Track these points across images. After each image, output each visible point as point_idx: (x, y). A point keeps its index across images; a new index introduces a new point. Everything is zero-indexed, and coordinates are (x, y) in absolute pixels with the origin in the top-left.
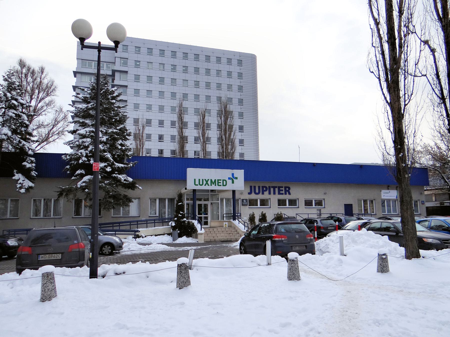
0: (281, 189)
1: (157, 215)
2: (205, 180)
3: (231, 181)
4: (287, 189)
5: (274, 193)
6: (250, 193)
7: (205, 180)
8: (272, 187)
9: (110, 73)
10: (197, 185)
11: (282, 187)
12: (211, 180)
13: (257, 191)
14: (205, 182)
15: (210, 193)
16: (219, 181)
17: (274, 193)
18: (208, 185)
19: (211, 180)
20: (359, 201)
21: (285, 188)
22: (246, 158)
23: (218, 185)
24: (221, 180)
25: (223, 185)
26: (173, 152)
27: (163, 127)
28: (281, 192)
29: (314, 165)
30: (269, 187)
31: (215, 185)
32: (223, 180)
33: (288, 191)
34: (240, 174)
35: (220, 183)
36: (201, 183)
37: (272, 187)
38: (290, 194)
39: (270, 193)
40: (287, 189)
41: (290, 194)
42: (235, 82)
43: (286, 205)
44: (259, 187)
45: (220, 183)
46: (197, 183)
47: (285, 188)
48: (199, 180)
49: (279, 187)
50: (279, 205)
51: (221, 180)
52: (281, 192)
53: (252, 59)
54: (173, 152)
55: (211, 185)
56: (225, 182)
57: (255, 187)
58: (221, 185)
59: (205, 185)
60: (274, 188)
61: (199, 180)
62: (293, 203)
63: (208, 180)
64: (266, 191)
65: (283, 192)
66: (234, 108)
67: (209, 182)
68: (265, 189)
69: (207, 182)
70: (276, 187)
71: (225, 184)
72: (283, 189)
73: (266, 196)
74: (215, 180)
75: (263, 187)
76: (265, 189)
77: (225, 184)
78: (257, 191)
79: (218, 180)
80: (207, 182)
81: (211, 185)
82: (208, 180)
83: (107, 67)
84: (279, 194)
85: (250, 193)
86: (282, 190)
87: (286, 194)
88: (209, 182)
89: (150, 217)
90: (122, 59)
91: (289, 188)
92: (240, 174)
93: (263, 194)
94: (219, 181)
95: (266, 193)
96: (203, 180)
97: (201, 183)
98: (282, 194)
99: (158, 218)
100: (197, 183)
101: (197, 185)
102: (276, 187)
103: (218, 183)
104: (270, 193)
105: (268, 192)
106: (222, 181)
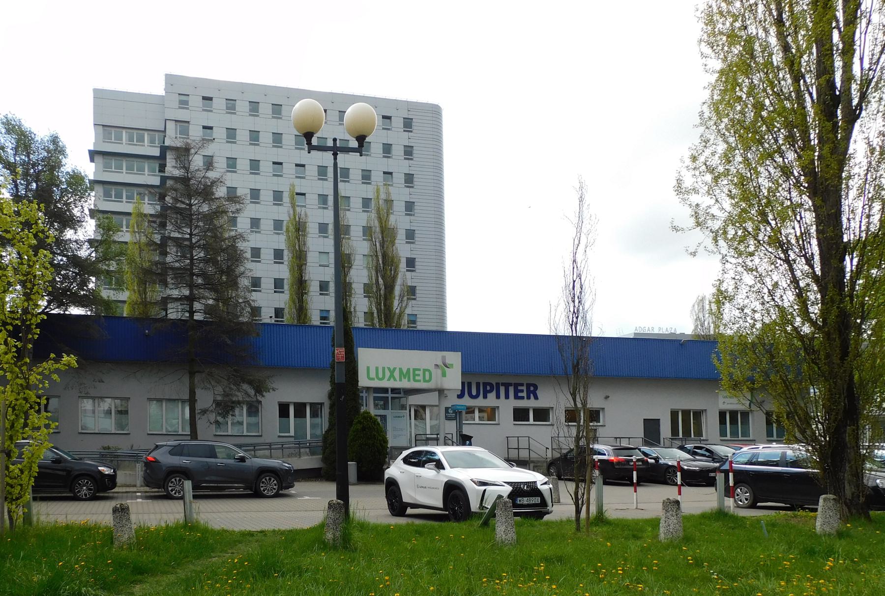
0: (520, 388)
1: (292, 433)
2: (389, 368)
3: (439, 371)
4: (532, 388)
5: (507, 397)
6: (461, 396)
7: (389, 368)
8: (503, 384)
9: (156, 152)
10: (373, 379)
11: (522, 385)
12: (401, 369)
13: (474, 393)
14: (388, 374)
15: (390, 395)
16: (417, 372)
17: (507, 397)
18: (395, 380)
19: (401, 369)
20: (674, 414)
21: (528, 386)
22: (420, 326)
23: (415, 380)
24: (419, 370)
25: (425, 381)
26: (279, 312)
27: (259, 262)
28: (520, 394)
29: (604, 338)
30: (498, 384)
31: (409, 380)
32: (425, 370)
33: (532, 392)
34: (454, 358)
35: (419, 375)
36: (381, 376)
37: (503, 384)
38: (536, 398)
39: (498, 397)
40: (532, 388)
41: (536, 398)
42: (399, 165)
43: (528, 420)
44: (478, 384)
45: (419, 375)
46: (373, 374)
47: (528, 386)
48: (377, 368)
49: (516, 386)
50: (646, 422)
51: (419, 370)
52: (520, 394)
53: (434, 113)
54: (279, 312)
55: (401, 380)
56: (427, 373)
57: (470, 384)
58: (419, 381)
59: (389, 380)
60: (507, 386)
61: (377, 368)
62: (542, 415)
63: (395, 369)
64: (491, 391)
65: (524, 394)
66: (399, 221)
67: (397, 374)
68: (488, 388)
69: (392, 372)
70: (510, 384)
71: (427, 378)
72: (524, 388)
73: (491, 401)
74: (408, 370)
75: (485, 384)
76: (488, 388)
77: (427, 378)
78: (474, 393)
79: (414, 370)
80: (392, 372)
81: (401, 380)
82: (395, 369)
83: (152, 141)
84: (517, 397)
85: (461, 396)
86: (522, 391)
87: (528, 398)
88: (397, 374)
89: (279, 437)
90: (178, 124)
91: (536, 387)
92: (454, 358)
93: (485, 397)
94: (417, 372)
95: (492, 396)
96: (384, 369)
97: (381, 376)
98: (522, 398)
99: (292, 439)
100: (373, 374)
101: (373, 379)
102: (510, 384)
103: (415, 375)
104: (498, 397)
105: (494, 393)
106: (421, 373)
